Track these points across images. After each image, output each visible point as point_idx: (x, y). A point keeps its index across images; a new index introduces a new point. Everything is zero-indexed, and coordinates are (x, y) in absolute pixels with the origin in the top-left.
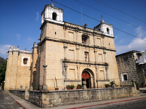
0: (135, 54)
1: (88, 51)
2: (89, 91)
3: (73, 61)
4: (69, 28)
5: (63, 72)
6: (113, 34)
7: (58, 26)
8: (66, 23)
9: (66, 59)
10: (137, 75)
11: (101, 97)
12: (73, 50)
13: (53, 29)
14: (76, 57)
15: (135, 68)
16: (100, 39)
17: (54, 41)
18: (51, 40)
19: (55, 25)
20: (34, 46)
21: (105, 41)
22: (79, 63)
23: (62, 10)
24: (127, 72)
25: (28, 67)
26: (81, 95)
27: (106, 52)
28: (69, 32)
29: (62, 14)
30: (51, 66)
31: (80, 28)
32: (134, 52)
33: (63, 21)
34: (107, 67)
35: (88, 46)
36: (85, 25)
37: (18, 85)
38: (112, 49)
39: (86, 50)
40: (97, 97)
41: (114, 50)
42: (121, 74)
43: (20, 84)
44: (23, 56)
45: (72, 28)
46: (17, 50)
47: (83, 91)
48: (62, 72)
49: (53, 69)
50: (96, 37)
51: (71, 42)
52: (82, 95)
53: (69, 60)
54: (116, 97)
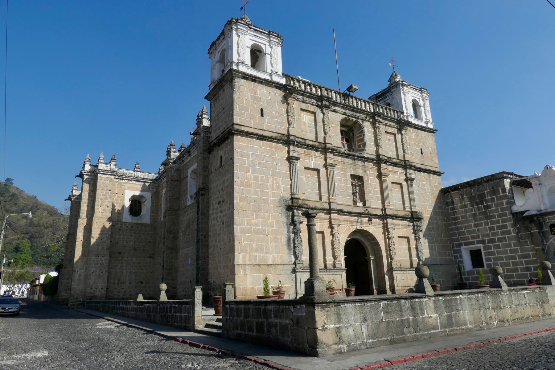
0: (507, 183)
1: (360, 173)
2: (438, 300)
4: (302, 95)
5: (289, 240)
6: (431, 121)
7: (268, 88)
8: (293, 79)
9: (296, 196)
10: (516, 250)
11: (472, 320)
13: (256, 99)
15: (509, 228)
17: (258, 139)
18: (248, 135)
19: (260, 86)
20: (84, 168)
21: (408, 141)
23: (279, 37)
24: (483, 242)
25: (145, 225)
26: (419, 311)
27: (413, 176)
28: (302, 110)
29: (277, 51)
30: (253, 221)
31: (334, 97)
32: (506, 178)
33: (284, 75)
34: (417, 226)
36: (350, 89)
37: (114, 284)
38: (431, 168)
39: (355, 170)
40: (462, 317)
41: (436, 170)
42: (462, 247)
43: (119, 280)
44: (129, 188)
45: (309, 97)
46: (109, 168)
47: (422, 297)
48: (285, 240)
49: (257, 232)
52: (423, 314)
53: (306, 202)
54: (509, 318)
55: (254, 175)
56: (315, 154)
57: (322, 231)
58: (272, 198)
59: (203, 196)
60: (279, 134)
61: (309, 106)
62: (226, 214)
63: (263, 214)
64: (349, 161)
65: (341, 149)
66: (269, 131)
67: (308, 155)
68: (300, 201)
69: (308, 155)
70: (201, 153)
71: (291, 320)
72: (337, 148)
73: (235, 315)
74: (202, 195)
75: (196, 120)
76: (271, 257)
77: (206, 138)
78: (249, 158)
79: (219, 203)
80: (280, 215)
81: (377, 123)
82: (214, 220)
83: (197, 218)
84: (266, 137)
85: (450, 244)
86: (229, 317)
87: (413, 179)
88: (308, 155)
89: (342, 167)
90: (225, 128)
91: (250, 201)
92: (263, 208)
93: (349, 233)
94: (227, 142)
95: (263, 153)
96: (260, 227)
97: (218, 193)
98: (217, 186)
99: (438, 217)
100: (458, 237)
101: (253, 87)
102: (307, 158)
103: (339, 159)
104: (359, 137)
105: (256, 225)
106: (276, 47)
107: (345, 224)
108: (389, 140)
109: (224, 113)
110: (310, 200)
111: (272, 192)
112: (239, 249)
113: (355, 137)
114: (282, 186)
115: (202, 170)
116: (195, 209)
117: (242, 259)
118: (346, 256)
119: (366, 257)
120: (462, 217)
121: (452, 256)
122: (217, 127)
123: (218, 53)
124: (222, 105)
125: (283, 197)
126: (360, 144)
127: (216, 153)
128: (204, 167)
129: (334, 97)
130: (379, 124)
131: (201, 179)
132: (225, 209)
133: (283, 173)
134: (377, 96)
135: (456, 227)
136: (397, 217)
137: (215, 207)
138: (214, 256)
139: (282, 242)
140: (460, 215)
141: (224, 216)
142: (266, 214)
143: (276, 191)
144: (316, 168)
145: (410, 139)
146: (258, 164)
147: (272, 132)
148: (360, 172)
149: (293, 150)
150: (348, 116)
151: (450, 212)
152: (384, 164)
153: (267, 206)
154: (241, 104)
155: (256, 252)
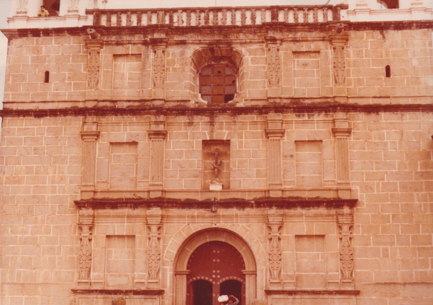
12: (134, 144)
38: (403, 102)
51: (125, 105)
57: (131, 234)
58: (50, 195)
63: (36, 218)
69: (119, 123)
88: (119, 123)
91: (18, 202)
102: (116, 128)
105: (24, 232)
108: (305, 65)
111: (52, 186)
119: (242, 271)
142: (39, 217)
143: (58, 183)
144: (131, 141)
145: (359, 53)
146: (35, 150)
155: (21, 268)
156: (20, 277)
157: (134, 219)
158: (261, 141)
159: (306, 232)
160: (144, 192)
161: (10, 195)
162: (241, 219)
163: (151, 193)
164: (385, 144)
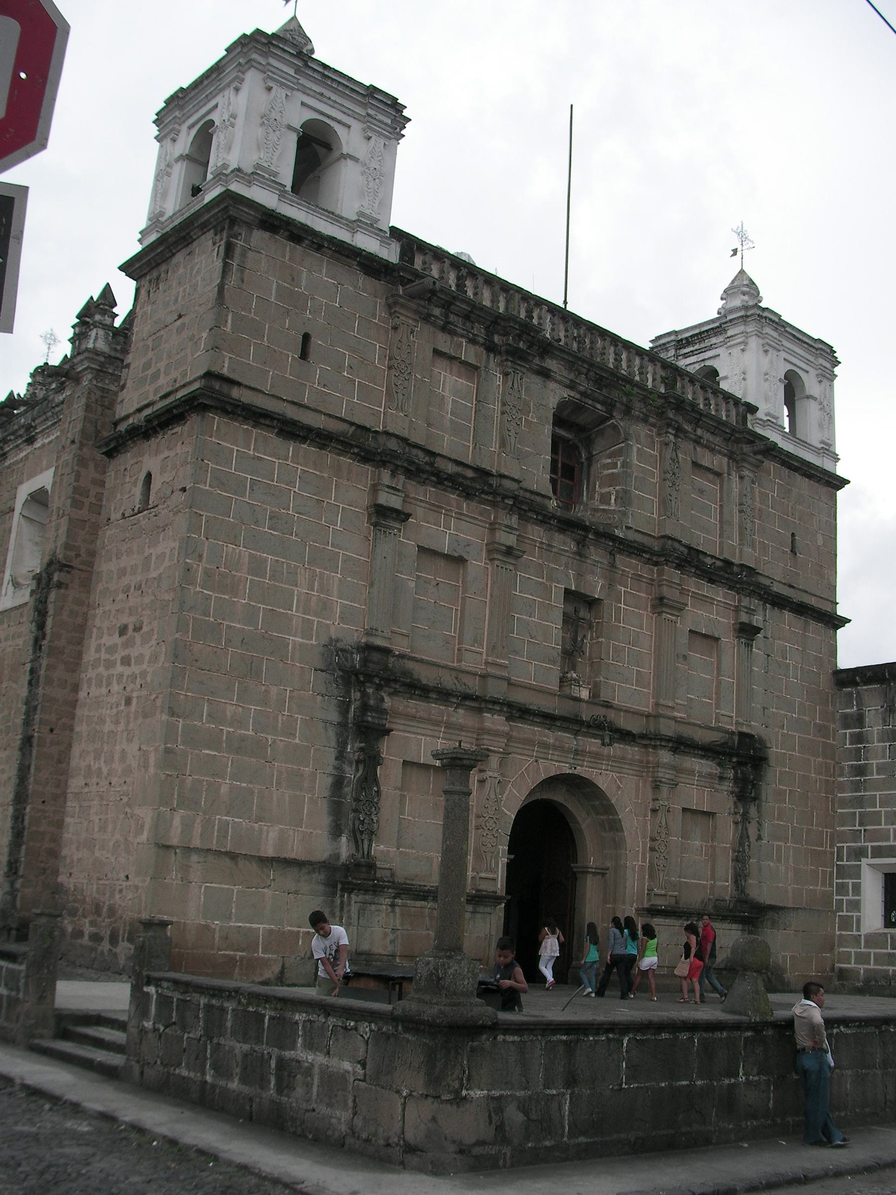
3: (448, 681)
9: (379, 642)
12: (460, 561)
14: (477, 641)
16: (718, 474)
22: (510, 705)
27: (757, 620)
30: (230, 710)
35: (605, 536)
39: (579, 575)
42: (864, 861)
48: (323, 784)
50: (686, 452)
51: (451, 468)
53: (410, 665)
55: (250, 555)
56: (459, 507)
59: (62, 591)
60: (352, 424)
61: (460, 345)
62: (144, 674)
63: (266, 691)
64: (565, 543)
65: (546, 501)
66: (321, 412)
67: (436, 508)
68: (392, 659)
70: (73, 442)
71: (359, 1062)
72: (533, 497)
73: (174, 1020)
74: (60, 585)
75: (73, 327)
76: (273, 834)
77: (99, 393)
78: (244, 496)
79: (123, 631)
80: (319, 698)
81: (670, 430)
82: (99, 685)
83: (32, 661)
84: (309, 429)
85: (832, 846)
86: (154, 1023)
87: (758, 630)
89: (540, 561)
90: (175, 381)
91: (229, 641)
92: (267, 668)
93: (531, 783)
94: (178, 429)
95: (292, 483)
96: (251, 733)
97: (122, 596)
98: (123, 572)
99: (812, 759)
100: (857, 828)
101: (290, 260)
103: (536, 533)
104: (607, 466)
105: (238, 722)
106: (382, 141)
107: (526, 752)
108: (701, 492)
109: (180, 331)
110: (422, 661)
112: (173, 794)
113: (596, 467)
114: (339, 603)
115: (69, 501)
116: (27, 629)
117: (179, 830)
118: (512, 857)
120: (880, 770)
121: (831, 885)
122: (150, 372)
123: (191, 127)
124: (176, 301)
125: (337, 640)
126: (607, 490)
127: (135, 460)
128: (76, 490)
129: (548, 326)
130: (676, 436)
131: (63, 529)
132: (142, 655)
133: (347, 559)
134: (681, 340)
135: (856, 798)
136: (687, 746)
137: (107, 640)
138: (86, 804)
139: (314, 788)
140: (874, 762)
141: (134, 677)
142: (274, 690)
143: (316, 616)
144: (456, 555)
145: (764, 497)
147: (330, 416)
148: (596, 587)
149: (388, 487)
150: (584, 394)
151: (848, 746)
152: (676, 568)
153: (281, 665)
154: (243, 309)
156: (226, 837)
157: (456, 732)
158: (645, 614)
159: (697, 804)
160: (475, 674)
161: (212, 619)
162: (614, 764)
163: (490, 681)
164: (788, 666)
